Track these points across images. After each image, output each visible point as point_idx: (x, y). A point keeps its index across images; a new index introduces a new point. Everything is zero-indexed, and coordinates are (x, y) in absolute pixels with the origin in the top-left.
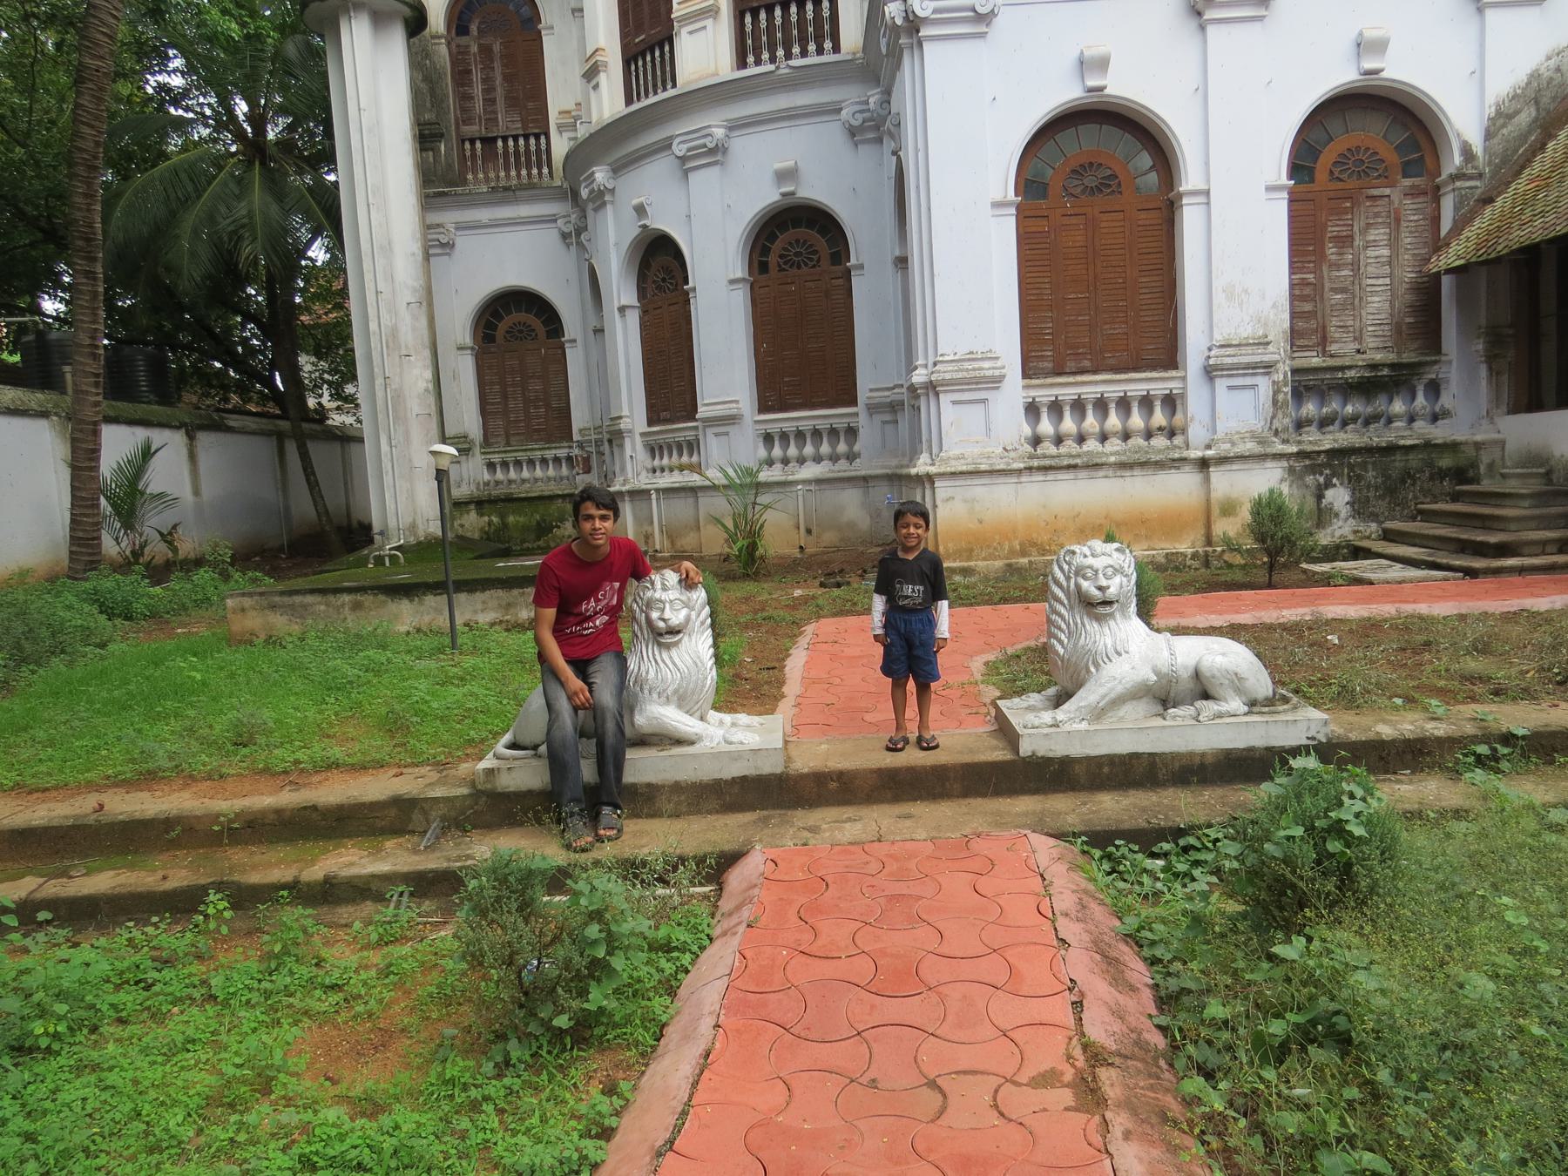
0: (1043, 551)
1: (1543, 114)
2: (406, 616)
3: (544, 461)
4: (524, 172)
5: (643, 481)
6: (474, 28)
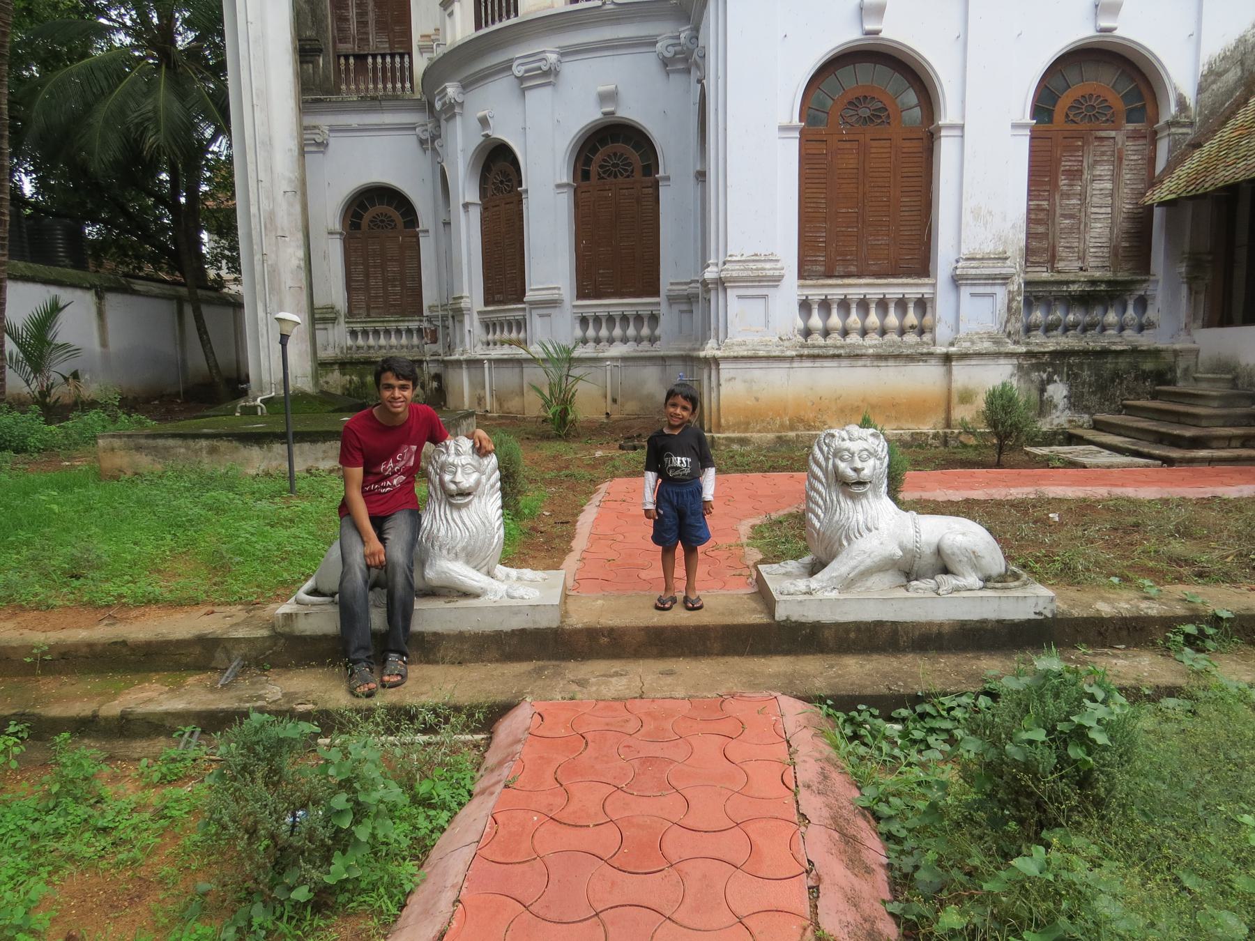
0: (809, 427)
1: (1247, 74)
2: (259, 461)
3: (398, 331)
4: (389, 86)
5: (479, 352)
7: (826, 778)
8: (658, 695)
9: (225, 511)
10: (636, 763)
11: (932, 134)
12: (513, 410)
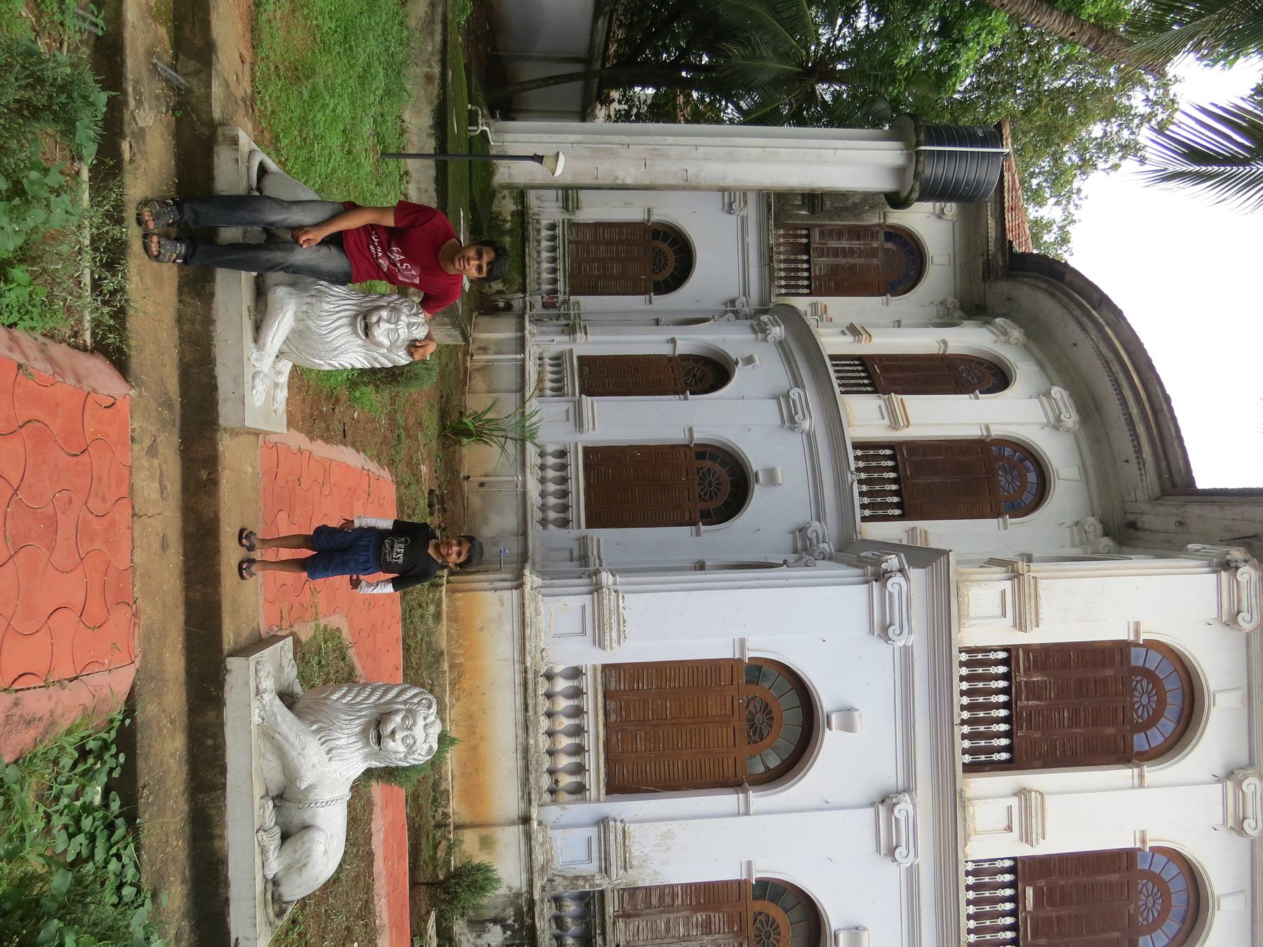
0: (453, 684)
2: (418, 124)
3: (554, 271)
4: (783, 274)
5: (532, 349)
6: (889, 245)
7: (29, 723)
9: (362, 84)
10: (50, 510)
12: (473, 382)
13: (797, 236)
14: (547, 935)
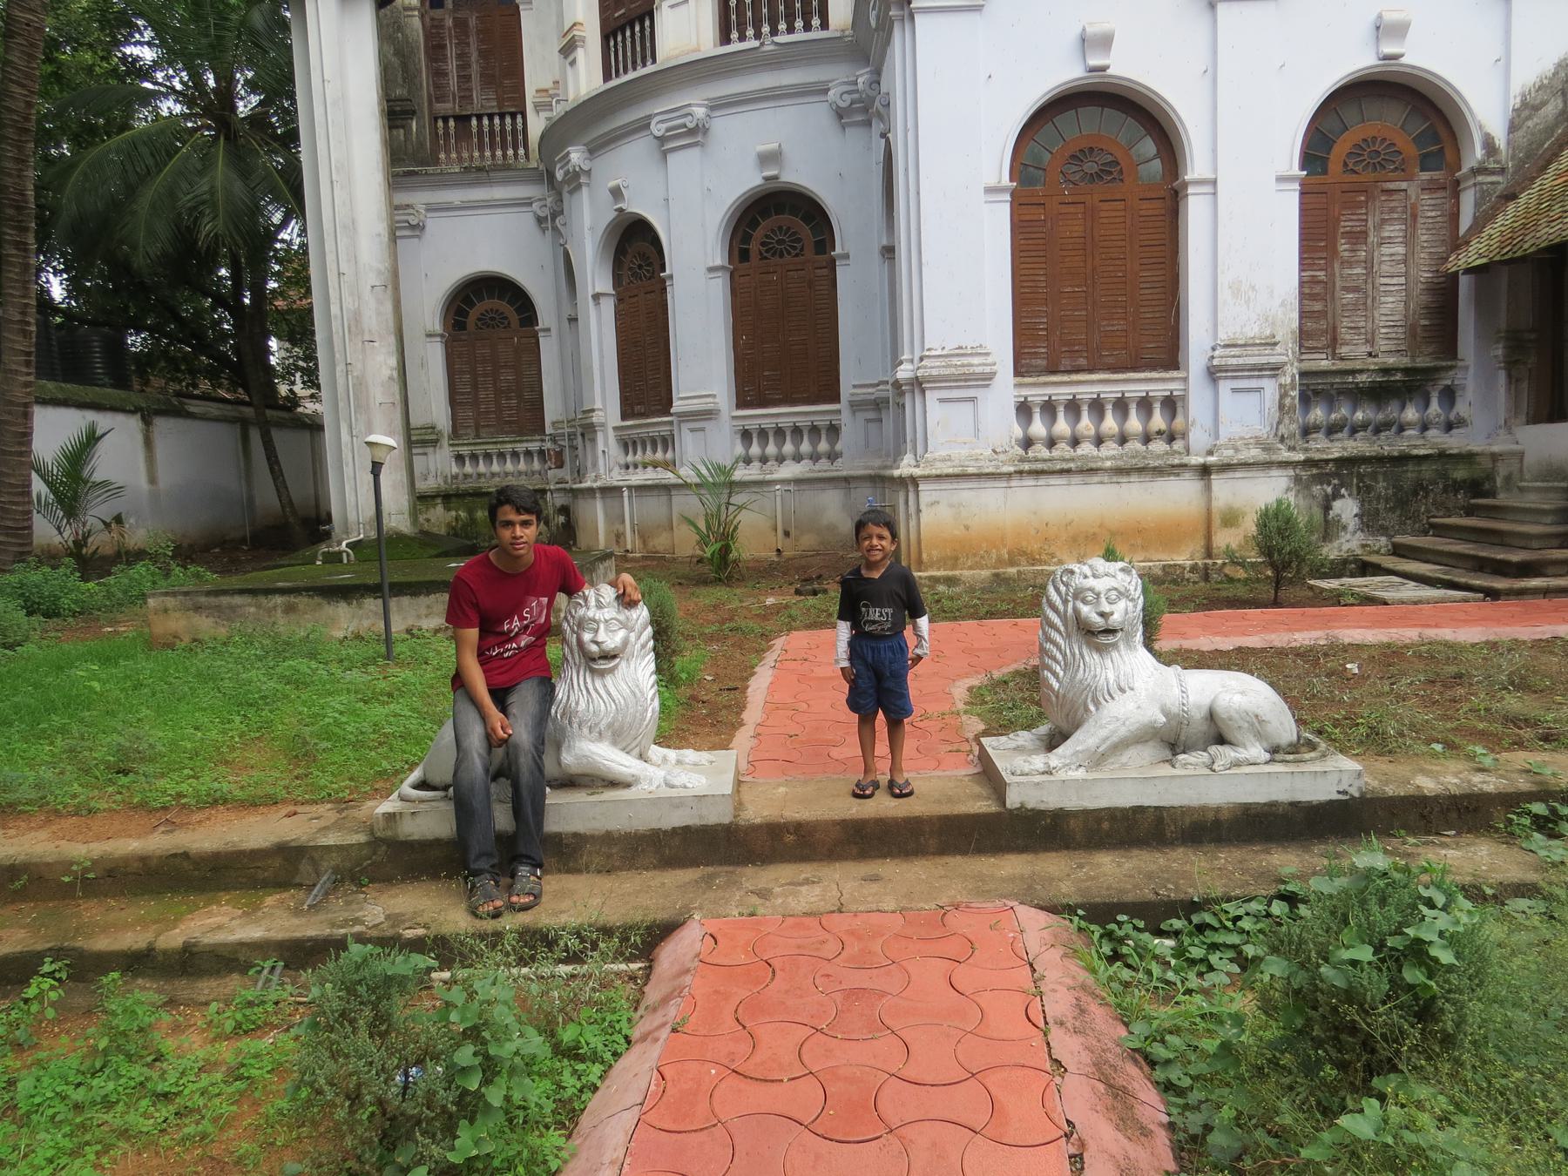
0: (1034, 561)
2: (347, 621)
3: (515, 455)
4: (499, 153)
5: (616, 478)
8: (862, 908)
9: (307, 685)
10: (838, 997)
11: (1176, 193)
13: (446, 134)
14: (1350, 444)
